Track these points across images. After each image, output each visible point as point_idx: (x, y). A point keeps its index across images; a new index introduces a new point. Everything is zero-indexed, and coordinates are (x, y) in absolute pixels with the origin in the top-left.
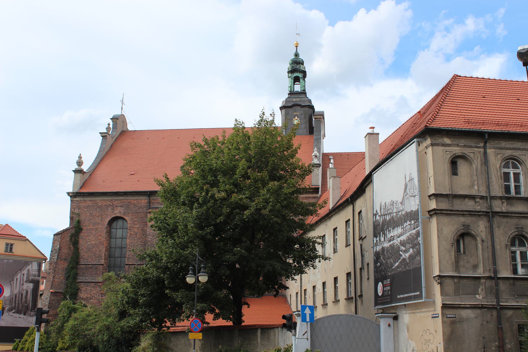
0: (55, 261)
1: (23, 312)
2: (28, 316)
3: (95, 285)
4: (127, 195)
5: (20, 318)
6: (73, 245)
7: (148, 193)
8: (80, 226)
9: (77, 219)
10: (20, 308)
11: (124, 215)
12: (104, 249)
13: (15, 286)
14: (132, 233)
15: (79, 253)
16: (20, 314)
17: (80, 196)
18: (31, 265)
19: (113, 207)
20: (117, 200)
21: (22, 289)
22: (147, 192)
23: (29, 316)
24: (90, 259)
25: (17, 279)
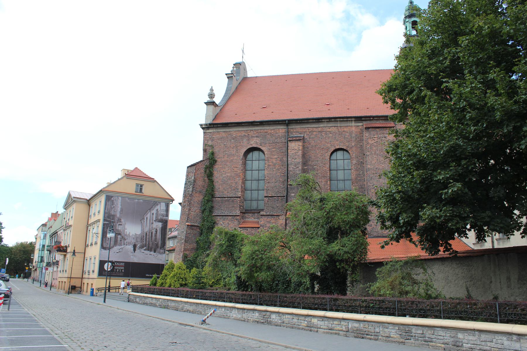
0: (190, 193)
1: (153, 250)
2: (158, 254)
3: (232, 218)
4: (264, 125)
5: (151, 255)
6: (208, 177)
7: (287, 122)
8: (214, 158)
9: (211, 151)
10: (150, 246)
11: (261, 145)
12: (241, 181)
13: (145, 224)
14: (270, 164)
15: (214, 186)
16: (151, 251)
17: (213, 127)
18: (159, 205)
19: (249, 138)
20: (252, 130)
21: (152, 227)
22: (285, 121)
23: (159, 253)
24: (226, 192)
25: (147, 218)
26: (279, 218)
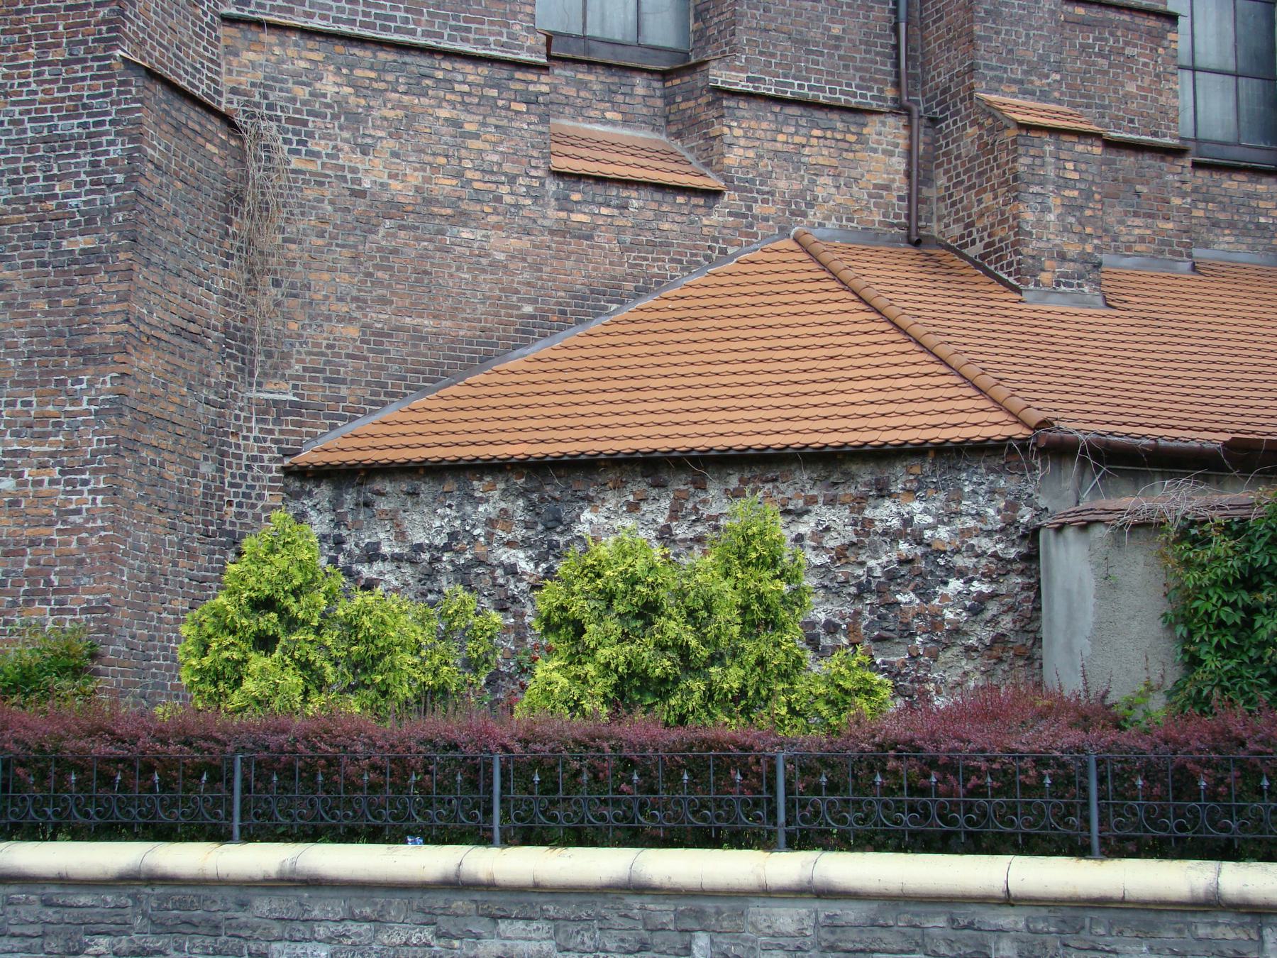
26: (862, 139)
